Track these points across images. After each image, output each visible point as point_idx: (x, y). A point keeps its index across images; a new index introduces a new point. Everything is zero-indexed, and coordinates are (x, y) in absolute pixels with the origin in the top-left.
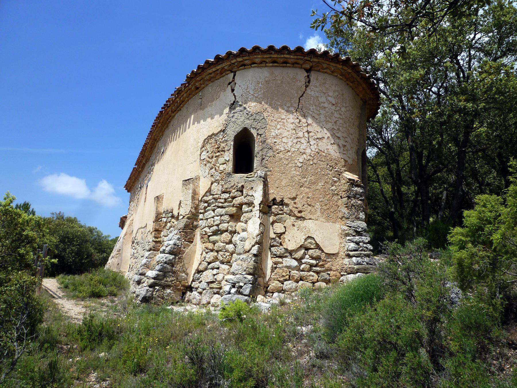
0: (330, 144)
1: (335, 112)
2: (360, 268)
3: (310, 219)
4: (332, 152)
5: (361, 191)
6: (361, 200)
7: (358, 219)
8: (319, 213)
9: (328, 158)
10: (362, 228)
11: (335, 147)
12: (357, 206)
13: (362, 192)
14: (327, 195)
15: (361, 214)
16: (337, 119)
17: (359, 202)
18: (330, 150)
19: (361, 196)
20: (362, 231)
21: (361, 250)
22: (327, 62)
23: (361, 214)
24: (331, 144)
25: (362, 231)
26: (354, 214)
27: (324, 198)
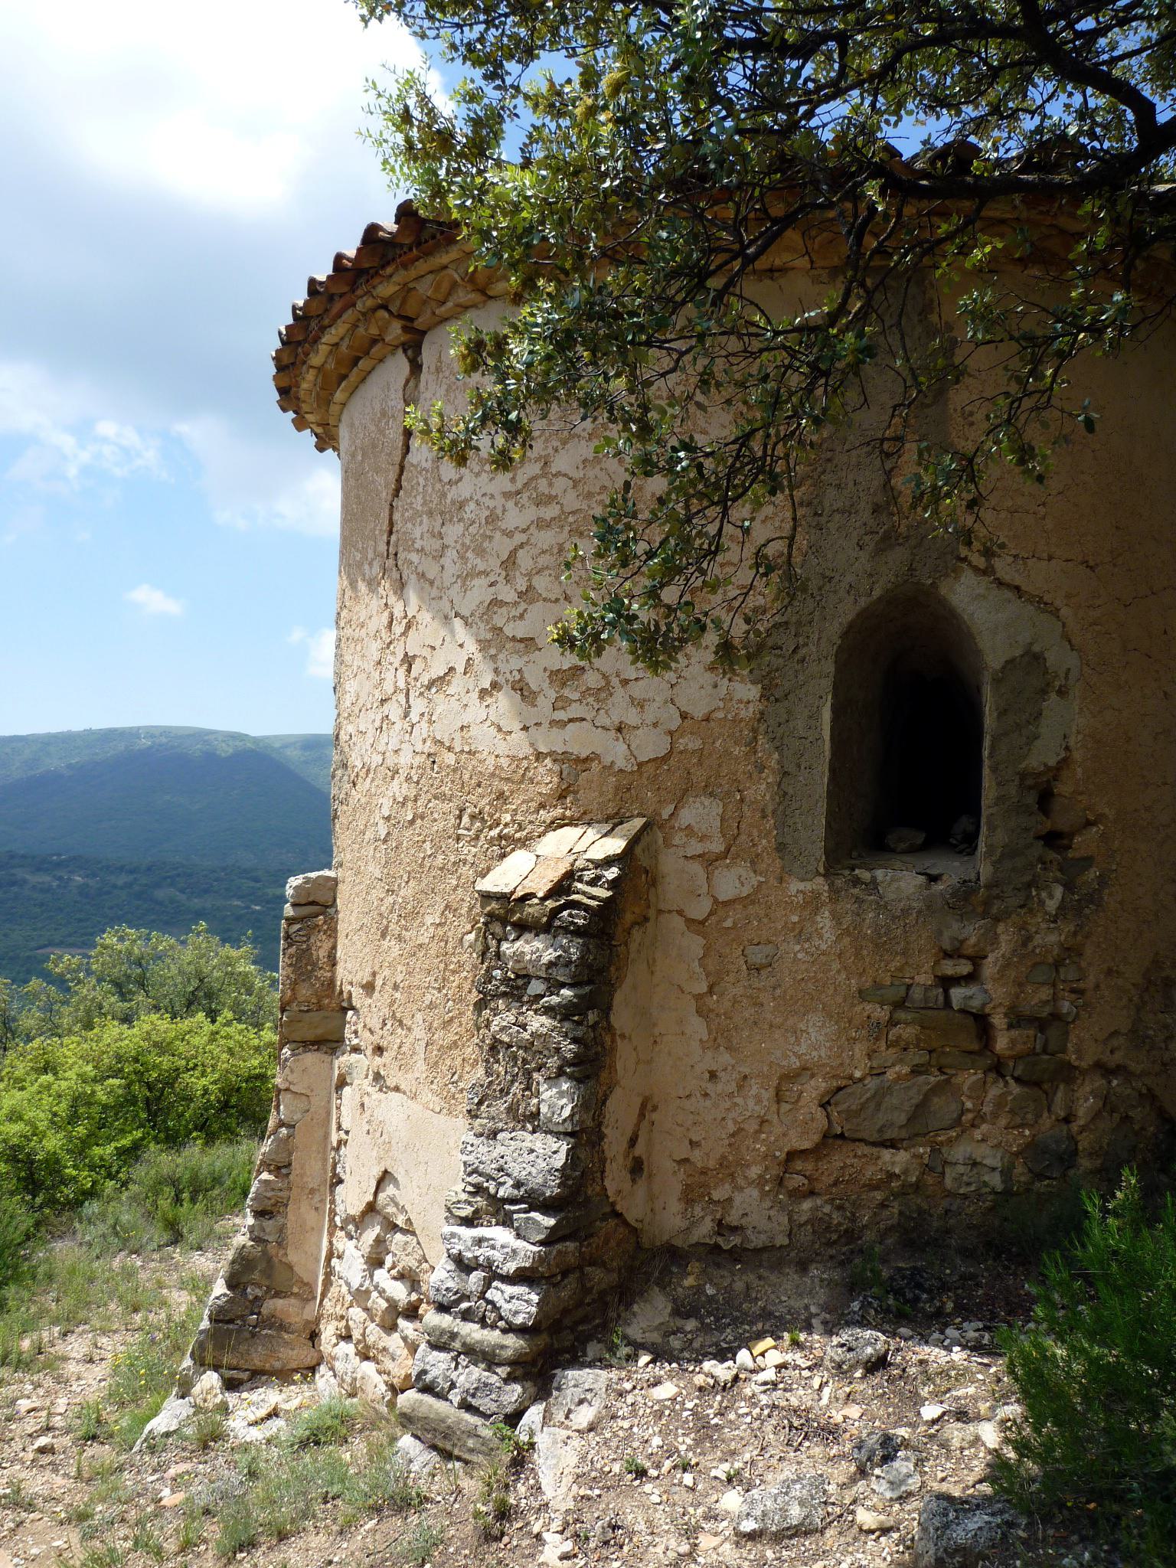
0: (475, 695)
1: (510, 504)
2: (422, 1411)
3: (397, 1089)
4: (485, 739)
5: (549, 955)
6: (549, 1010)
7: (532, 1120)
8: (420, 1067)
9: (466, 777)
10: (518, 1185)
11: (503, 703)
12: (527, 1047)
13: (551, 964)
14: (454, 972)
15: (548, 1093)
16: (520, 538)
17: (538, 1023)
18: (474, 731)
19: (554, 986)
20: (513, 1201)
21: (466, 1316)
22: (422, 266)
23: (548, 1093)
24: (483, 694)
25: (513, 1201)
26: (504, 1092)
27: (439, 990)
